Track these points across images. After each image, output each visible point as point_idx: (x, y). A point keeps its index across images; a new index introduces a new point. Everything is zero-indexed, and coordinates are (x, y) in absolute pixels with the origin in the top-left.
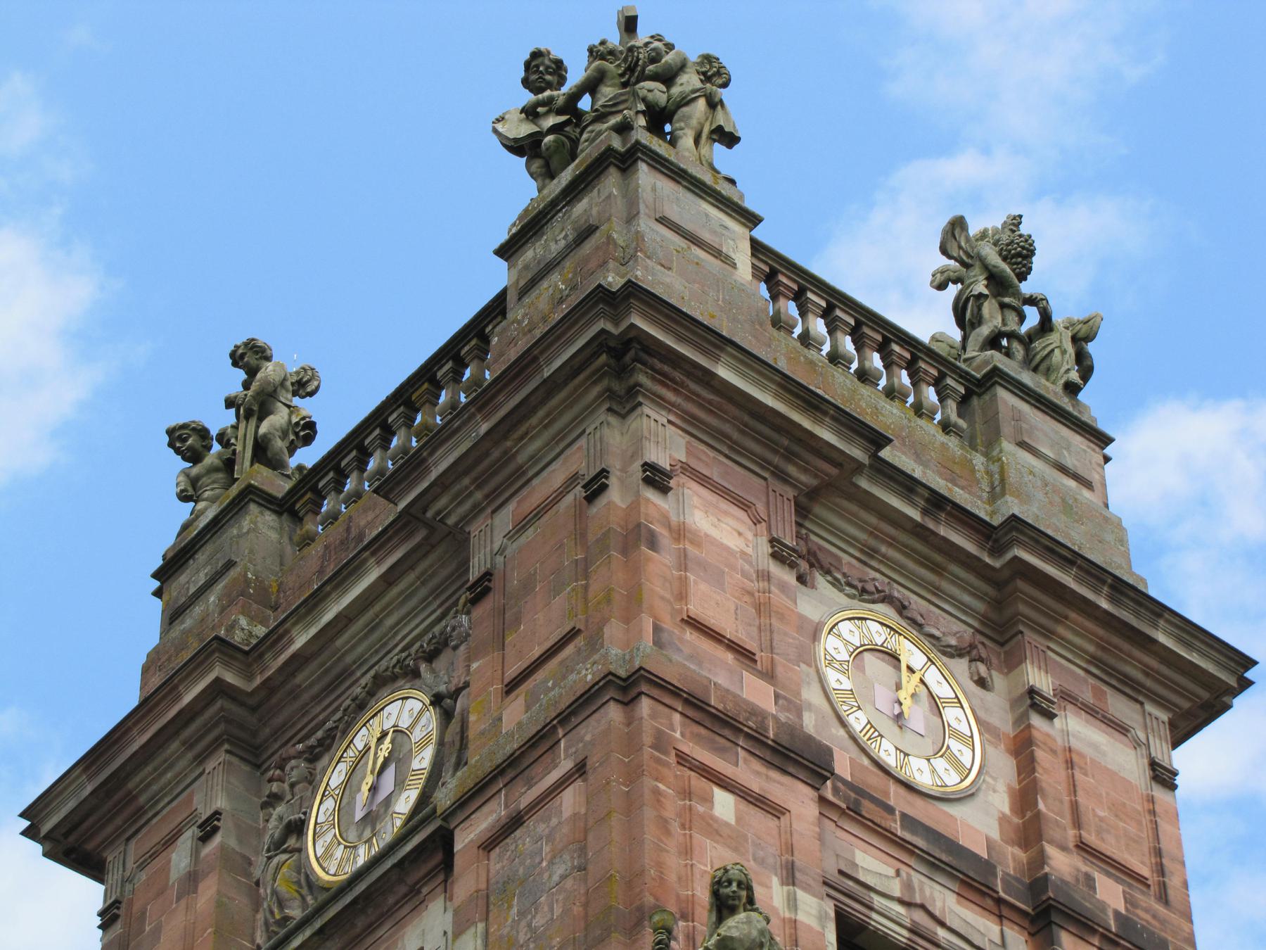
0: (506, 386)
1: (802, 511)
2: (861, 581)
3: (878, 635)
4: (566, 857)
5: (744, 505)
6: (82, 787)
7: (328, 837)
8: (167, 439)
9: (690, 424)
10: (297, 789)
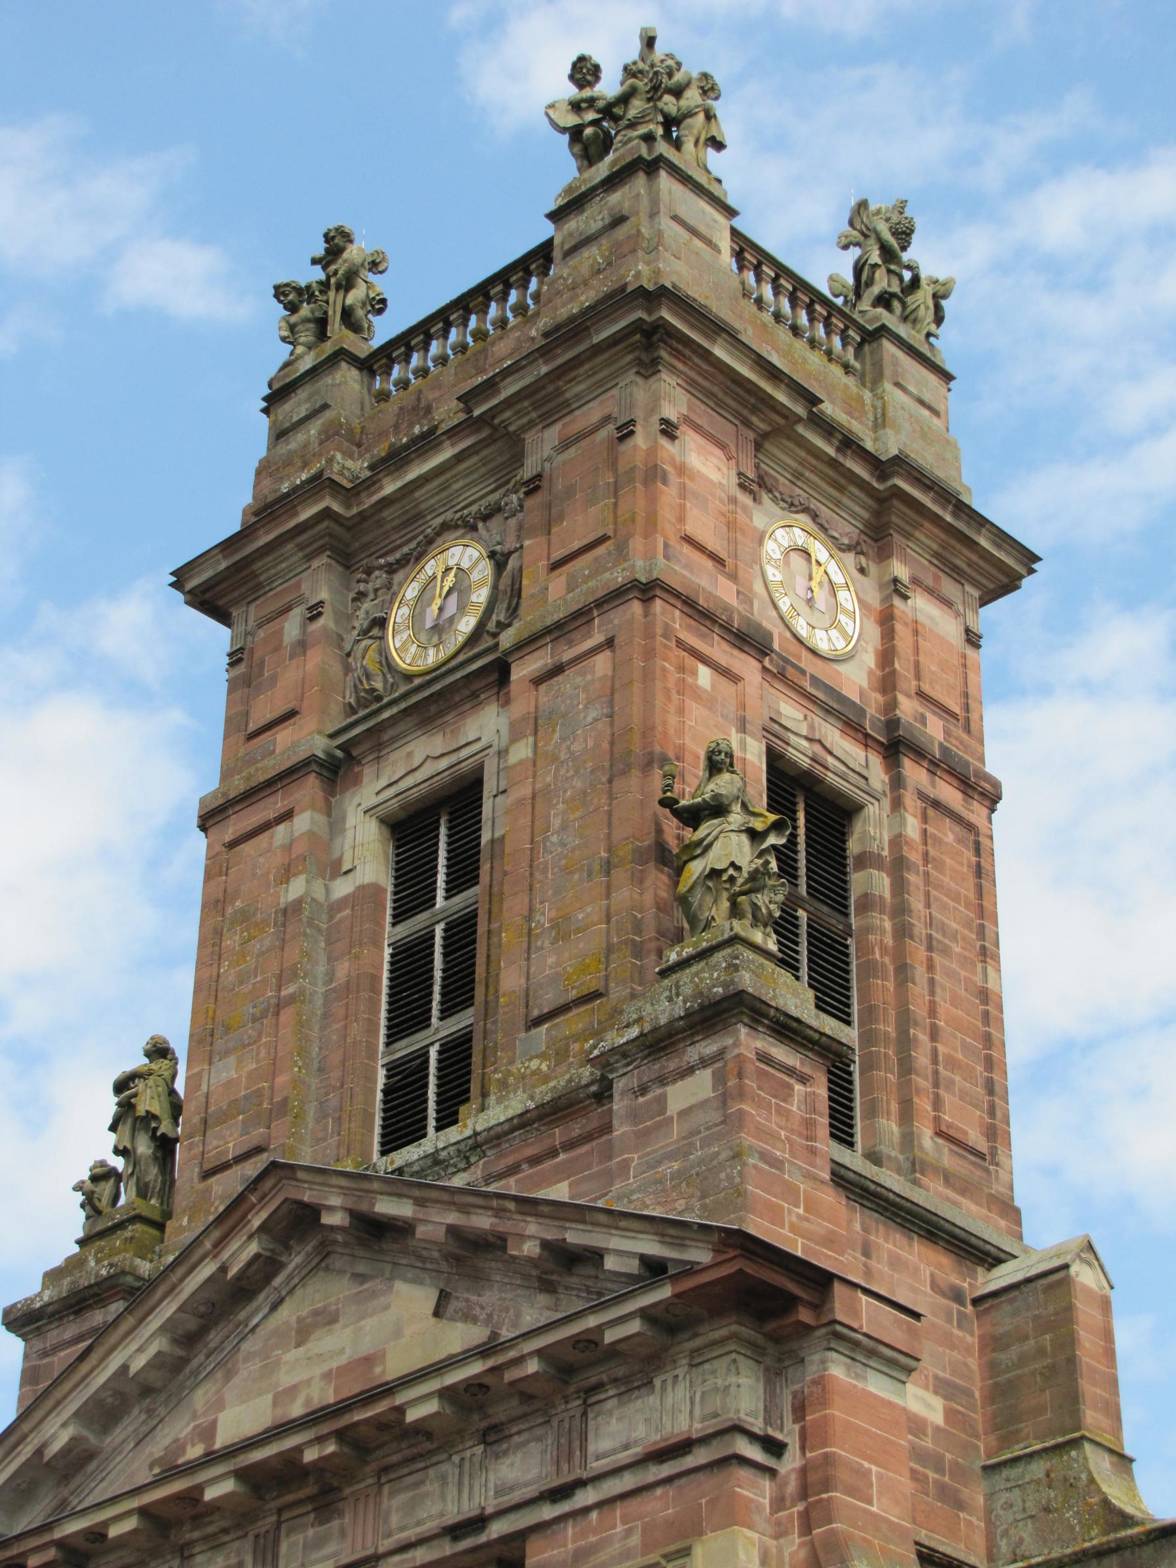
0: (565, 341)
1: (758, 447)
2: (791, 497)
3: (800, 538)
4: (598, 706)
5: (722, 446)
6: (218, 562)
7: (405, 636)
8: (273, 291)
9: (692, 386)
10: (380, 593)
